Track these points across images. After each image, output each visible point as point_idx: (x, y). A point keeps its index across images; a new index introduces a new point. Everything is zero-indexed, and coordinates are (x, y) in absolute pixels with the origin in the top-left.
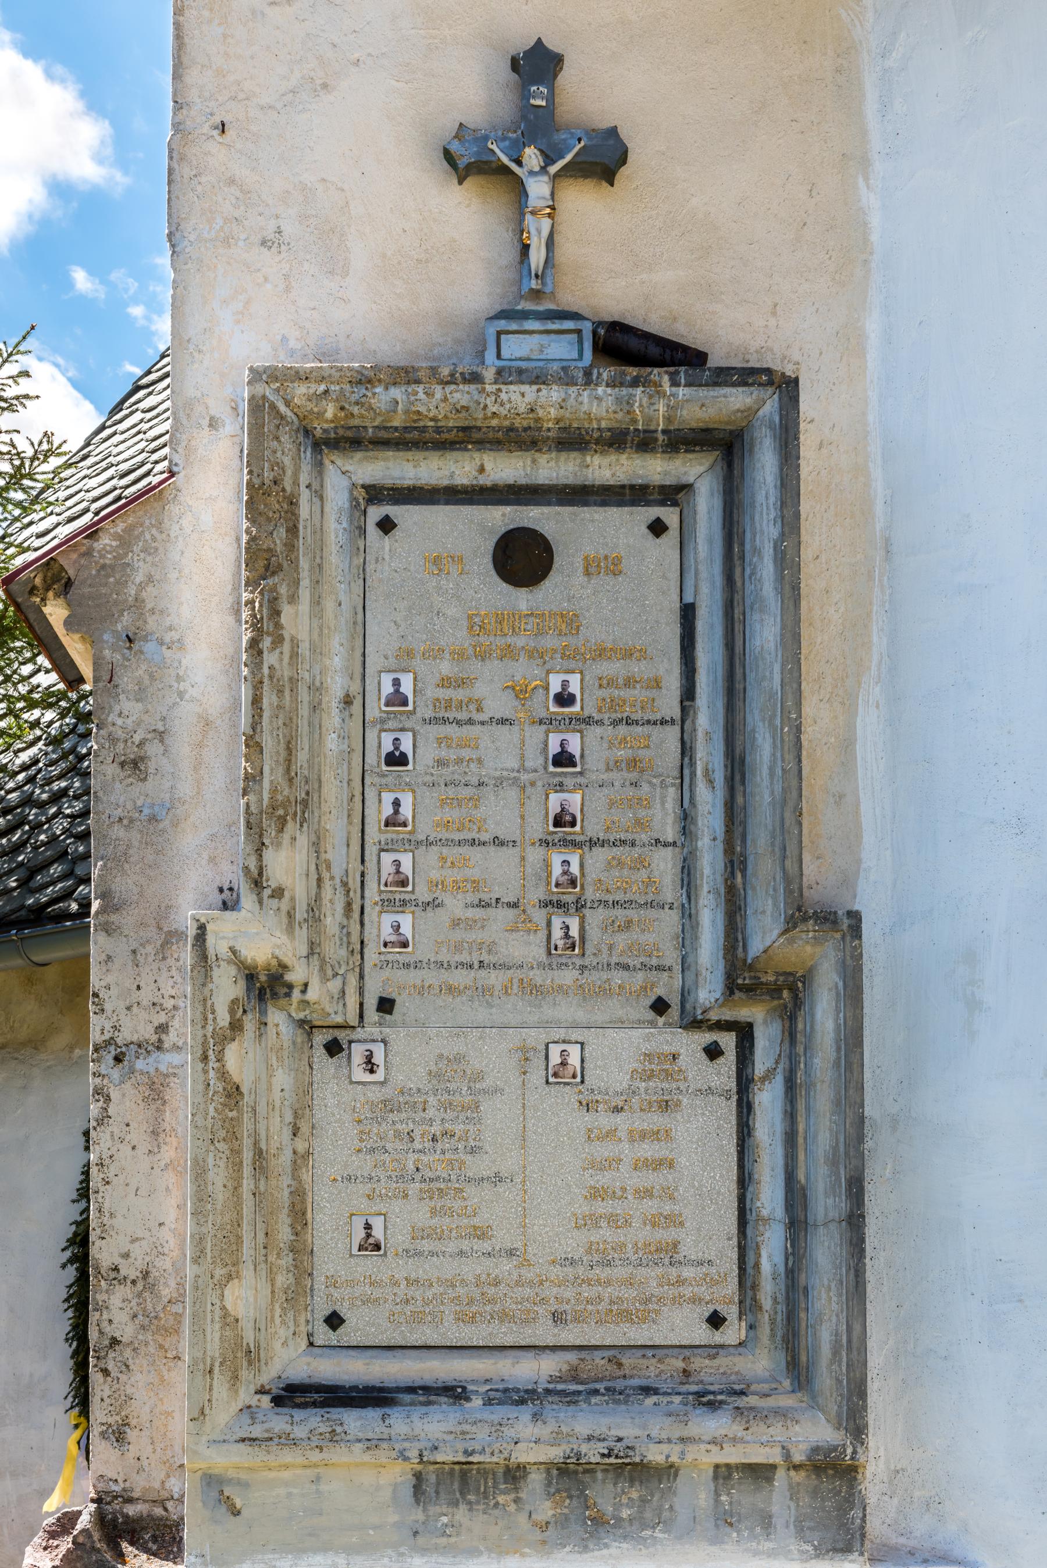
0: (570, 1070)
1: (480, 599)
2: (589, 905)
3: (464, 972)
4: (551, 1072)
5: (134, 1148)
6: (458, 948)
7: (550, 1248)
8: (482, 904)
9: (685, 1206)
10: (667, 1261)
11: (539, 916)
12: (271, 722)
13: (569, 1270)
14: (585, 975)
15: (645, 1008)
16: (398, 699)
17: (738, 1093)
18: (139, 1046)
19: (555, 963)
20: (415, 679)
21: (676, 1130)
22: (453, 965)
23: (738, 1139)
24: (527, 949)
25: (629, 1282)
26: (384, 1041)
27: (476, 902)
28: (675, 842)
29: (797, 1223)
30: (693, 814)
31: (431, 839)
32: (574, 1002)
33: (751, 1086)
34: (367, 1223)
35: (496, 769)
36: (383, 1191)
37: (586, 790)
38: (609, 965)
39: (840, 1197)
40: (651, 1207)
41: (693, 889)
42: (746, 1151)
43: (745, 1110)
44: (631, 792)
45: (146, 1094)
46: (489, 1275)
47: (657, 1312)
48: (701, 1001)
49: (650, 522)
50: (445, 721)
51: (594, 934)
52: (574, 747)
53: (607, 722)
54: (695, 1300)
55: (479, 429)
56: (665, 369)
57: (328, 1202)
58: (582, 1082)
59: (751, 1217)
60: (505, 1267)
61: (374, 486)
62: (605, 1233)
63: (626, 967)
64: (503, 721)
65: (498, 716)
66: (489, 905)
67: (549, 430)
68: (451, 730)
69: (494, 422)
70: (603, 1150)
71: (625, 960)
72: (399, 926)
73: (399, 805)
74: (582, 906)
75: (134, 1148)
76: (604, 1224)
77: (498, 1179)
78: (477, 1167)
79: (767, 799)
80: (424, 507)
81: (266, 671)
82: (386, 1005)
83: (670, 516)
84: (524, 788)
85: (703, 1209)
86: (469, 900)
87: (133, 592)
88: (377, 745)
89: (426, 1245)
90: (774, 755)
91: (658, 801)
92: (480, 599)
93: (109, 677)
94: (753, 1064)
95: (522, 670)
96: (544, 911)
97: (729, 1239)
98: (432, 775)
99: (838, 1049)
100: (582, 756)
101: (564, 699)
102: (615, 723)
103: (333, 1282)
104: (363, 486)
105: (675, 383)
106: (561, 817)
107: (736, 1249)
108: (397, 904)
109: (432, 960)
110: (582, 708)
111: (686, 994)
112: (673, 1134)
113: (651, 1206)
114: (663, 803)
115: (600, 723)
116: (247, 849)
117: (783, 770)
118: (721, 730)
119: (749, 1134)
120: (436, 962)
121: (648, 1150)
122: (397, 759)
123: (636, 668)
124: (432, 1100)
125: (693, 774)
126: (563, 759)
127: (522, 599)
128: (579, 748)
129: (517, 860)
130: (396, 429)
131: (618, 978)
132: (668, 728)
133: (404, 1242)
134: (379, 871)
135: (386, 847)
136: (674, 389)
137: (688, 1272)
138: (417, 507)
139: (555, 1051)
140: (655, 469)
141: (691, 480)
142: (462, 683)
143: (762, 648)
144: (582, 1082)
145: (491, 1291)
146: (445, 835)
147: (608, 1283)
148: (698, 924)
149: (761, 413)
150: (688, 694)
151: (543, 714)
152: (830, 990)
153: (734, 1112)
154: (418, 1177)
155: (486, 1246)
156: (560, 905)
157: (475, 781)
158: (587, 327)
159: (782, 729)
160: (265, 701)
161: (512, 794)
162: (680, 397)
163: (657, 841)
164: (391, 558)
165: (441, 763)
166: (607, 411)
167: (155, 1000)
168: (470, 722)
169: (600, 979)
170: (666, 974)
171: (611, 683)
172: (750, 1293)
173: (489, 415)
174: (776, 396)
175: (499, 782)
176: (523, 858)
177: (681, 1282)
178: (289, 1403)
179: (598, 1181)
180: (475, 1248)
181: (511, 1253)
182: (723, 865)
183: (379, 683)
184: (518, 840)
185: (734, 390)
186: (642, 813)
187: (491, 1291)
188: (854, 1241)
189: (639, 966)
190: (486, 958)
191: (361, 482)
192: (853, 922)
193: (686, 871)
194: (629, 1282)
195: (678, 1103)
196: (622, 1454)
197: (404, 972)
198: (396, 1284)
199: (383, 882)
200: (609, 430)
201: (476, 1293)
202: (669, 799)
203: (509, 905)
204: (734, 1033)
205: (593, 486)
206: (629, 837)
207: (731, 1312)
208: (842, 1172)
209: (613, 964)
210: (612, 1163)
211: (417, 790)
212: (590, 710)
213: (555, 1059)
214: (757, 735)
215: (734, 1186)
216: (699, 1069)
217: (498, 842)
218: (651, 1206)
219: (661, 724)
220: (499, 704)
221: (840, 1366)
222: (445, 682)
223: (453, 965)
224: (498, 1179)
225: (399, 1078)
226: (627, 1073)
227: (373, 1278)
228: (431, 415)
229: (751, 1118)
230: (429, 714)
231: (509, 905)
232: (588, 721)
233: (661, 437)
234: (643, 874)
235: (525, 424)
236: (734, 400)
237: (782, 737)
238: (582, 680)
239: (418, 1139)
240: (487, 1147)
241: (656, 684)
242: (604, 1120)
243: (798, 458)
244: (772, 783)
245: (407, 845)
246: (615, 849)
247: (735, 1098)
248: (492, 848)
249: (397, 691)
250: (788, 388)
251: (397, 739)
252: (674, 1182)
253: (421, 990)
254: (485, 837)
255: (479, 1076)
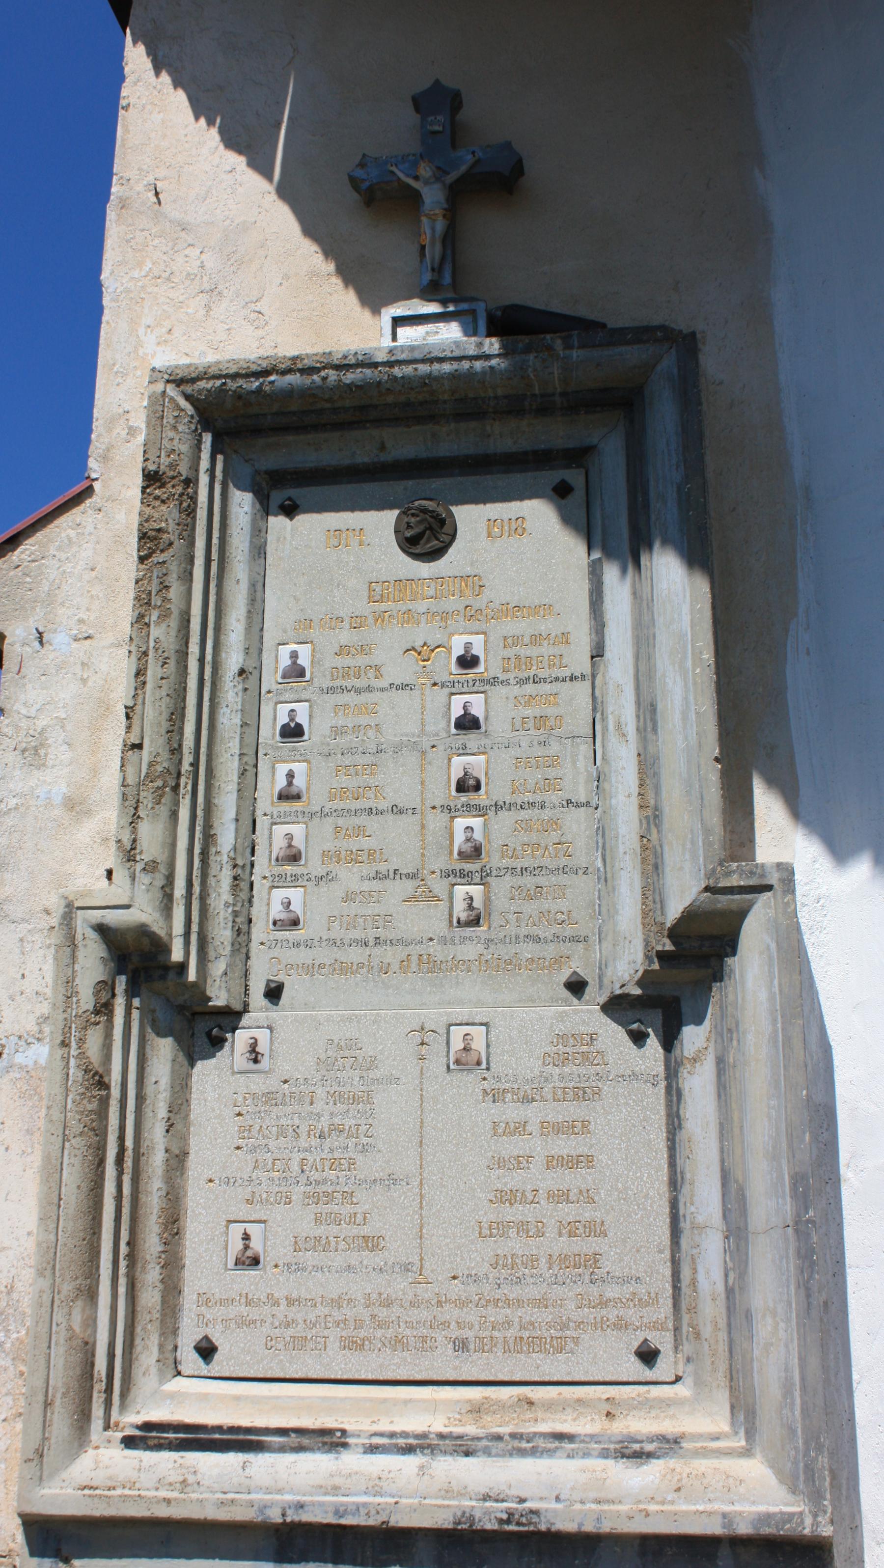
0: (473, 1057)
1: (381, 569)
2: (494, 873)
3: (359, 950)
4: (452, 1059)
5: (7, 1149)
6: (351, 925)
7: (451, 1263)
8: (378, 876)
9: (608, 1213)
10: (587, 1278)
11: (439, 886)
12: (153, 693)
13: (473, 1288)
14: (491, 950)
15: (558, 985)
16: (296, 672)
17: (667, 1078)
18: (20, 1037)
19: (457, 938)
20: (313, 650)
21: (596, 1123)
22: (346, 941)
23: (668, 1132)
24: (430, 921)
25: (542, 1303)
26: (270, 1028)
27: (373, 874)
28: (588, 802)
29: (737, 1231)
30: (606, 770)
31: (326, 810)
32: (479, 980)
33: (681, 1069)
34: (245, 1234)
35: (395, 735)
36: (264, 1196)
37: (491, 753)
38: (517, 937)
39: (784, 1197)
40: (568, 1214)
41: (608, 852)
42: (677, 1146)
43: (675, 1098)
44: (539, 751)
45: (23, 1090)
46: (380, 1294)
47: (576, 1341)
48: (620, 974)
49: (554, 484)
50: (343, 689)
51: (500, 902)
52: (477, 711)
53: (512, 682)
54: (621, 1325)
55: (375, 407)
56: (558, 334)
57: (204, 1208)
58: (488, 1069)
59: (685, 1225)
60: (400, 1286)
61: (277, 471)
62: (515, 1244)
63: (537, 940)
64: (404, 687)
65: (398, 682)
66: (386, 877)
67: (445, 402)
68: (349, 698)
69: (390, 399)
70: (511, 1147)
71: (535, 931)
72: (289, 903)
73: (293, 777)
74: (487, 875)
75: (7, 1149)
76: (512, 1232)
77: (393, 1180)
78: (370, 1166)
79: (681, 744)
80: (326, 487)
81: (152, 644)
82: (274, 993)
83: (575, 477)
84: (423, 753)
85: (629, 1216)
86: (365, 873)
87: (46, 589)
88: (272, 717)
89: (309, 1258)
90: (686, 699)
91: (569, 759)
92: (381, 569)
93: (17, 669)
94: (682, 1045)
95: (419, 635)
96: (446, 882)
97: (661, 1252)
98: (328, 745)
99: (774, 1021)
100: (486, 718)
101: (468, 662)
102: (523, 682)
103: (205, 1300)
104: (266, 472)
105: (568, 347)
106: (464, 782)
107: (669, 1264)
108: (289, 879)
109: (324, 938)
110: (486, 669)
111: (603, 967)
112: (592, 1127)
113: (568, 1212)
114: (574, 763)
115: (505, 683)
116: (122, 822)
117: (697, 713)
118: (632, 680)
119: (680, 1126)
120: (328, 940)
121: (564, 1146)
122: (292, 732)
123: (547, 625)
124: (320, 1092)
125: (605, 729)
126: (468, 723)
127: (424, 569)
128: (483, 709)
129: (418, 828)
130: (294, 413)
131: (528, 951)
132: (577, 684)
133: (285, 1255)
134: (271, 845)
135: (278, 820)
136: (567, 352)
137: (612, 1291)
138: (319, 488)
139: (457, 1033)
140: (556, 434)
141: (595, 441)
142: (363, 649)
143: (669, 590)
144: (488, 1069)
145: (383, 1313)
146: (338, 804)
147: (520, 1303)
148: (614, 889)
149: (659, 368)
150: (598, 653)
151: (445, 678)
152: (761, 953)
153: (662, 1101)
154: (303, 1179)
155: (377, 1259)
156: (463, 874)
157: (373, 748)
158: (481, 307)
159: (694, 670)
160: (149, 673)
161: (412, 759)
162: (574, 359)
163: (569, 802)
164: (292, 536)
165: (337, 731)
166: (502, 379)
167: (40, 989)
168: (369, 689)
169: (507, 954)
170: (581, 945)
171: (517, 640)
172: (686, 1319)
173: (384, 391)
174: (673, 351)
175: (397, 749)
176: (423, 827)
177: (604, 1303)
178: (141, 1445)
179: (506, 1184)
180: (365, 1262)
181: (406, 1268)
182: (637, 821)
183: (277, 657)
184: (419, 807)
185: (628, 348)
186: (551, 773)
187: (383, 1313)
188: (803, 1252)
189: (551, 938)
190: (380, 932)
191: (264, 468)
192: (785, 875)
193: (600, 832)
194: (542, 1303)
195: (598, 1092)
196: (524, 1520)
197: (294, 951)
198: (277, 1303)
199: (274, 857)
200: (506, 397)
201: (365, 1315)
202: (581, 757)
203: (408, 876)
204: (660, 1011)
205: (495, 454)
206: (538, 798)
207: (663, 1341)
208: (785, 1167)
209: (521, 936)
210: (521, 1162)
211: (312, 761)
212: (495, 671)
213: (457, 1044)
214: (667, 680)
215: (664, 1189)
216: (621, 1053)
217: (397, 810)
218: (568, 1212)
219: (571, 680)
220: (399, 669)
221: (792, 1410)
222: (343, 650)
223: (346, 941)
224: (393, 1180)
225: (285, 1068)
226: (538, 1058)
227: (250, 1297)
228: (327, 396)
229: (682, 1106)
230: (327, 683)
231: (408, 876)
232: (494, 681)
233: (558, 399)
234: (554, 836)
235: (420, 398)
236: (632, 355)
237: (694, 680)
238: (485, 642)
239: (304, 1135)
240: (380, 1146)
241: (565, 638)
242: (512, 1112)
243: (700, 404)
244: (685, 728)
245: (300, 817)
246: (523, 812)
247: (663, 1084)
248: (390, 817)
249: (294, 663)
250: (687, 344)
251: (292, 711)
252: (594, 1184)
253: (310, 969)
254: (383, 805)
255: (372, 1063)
